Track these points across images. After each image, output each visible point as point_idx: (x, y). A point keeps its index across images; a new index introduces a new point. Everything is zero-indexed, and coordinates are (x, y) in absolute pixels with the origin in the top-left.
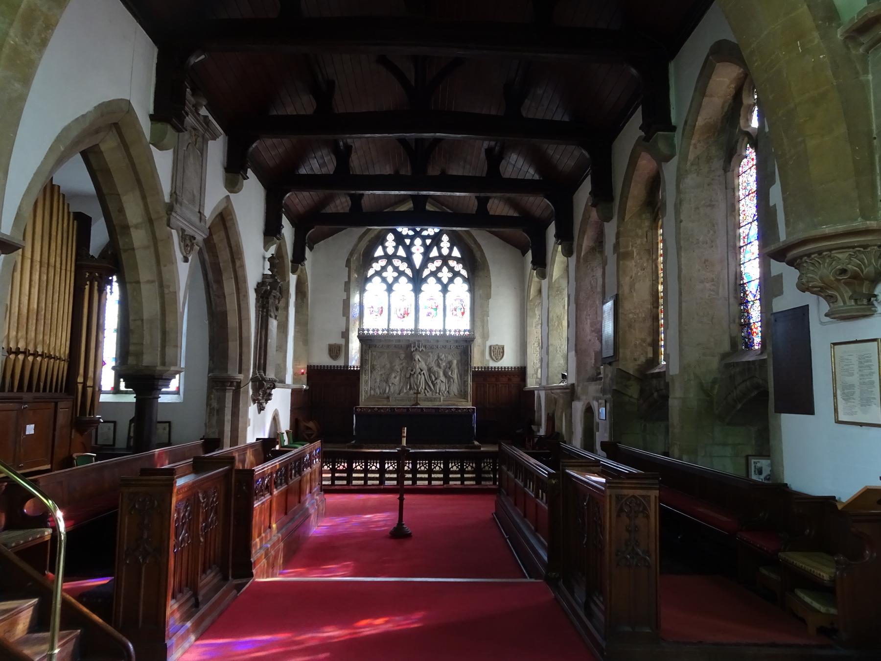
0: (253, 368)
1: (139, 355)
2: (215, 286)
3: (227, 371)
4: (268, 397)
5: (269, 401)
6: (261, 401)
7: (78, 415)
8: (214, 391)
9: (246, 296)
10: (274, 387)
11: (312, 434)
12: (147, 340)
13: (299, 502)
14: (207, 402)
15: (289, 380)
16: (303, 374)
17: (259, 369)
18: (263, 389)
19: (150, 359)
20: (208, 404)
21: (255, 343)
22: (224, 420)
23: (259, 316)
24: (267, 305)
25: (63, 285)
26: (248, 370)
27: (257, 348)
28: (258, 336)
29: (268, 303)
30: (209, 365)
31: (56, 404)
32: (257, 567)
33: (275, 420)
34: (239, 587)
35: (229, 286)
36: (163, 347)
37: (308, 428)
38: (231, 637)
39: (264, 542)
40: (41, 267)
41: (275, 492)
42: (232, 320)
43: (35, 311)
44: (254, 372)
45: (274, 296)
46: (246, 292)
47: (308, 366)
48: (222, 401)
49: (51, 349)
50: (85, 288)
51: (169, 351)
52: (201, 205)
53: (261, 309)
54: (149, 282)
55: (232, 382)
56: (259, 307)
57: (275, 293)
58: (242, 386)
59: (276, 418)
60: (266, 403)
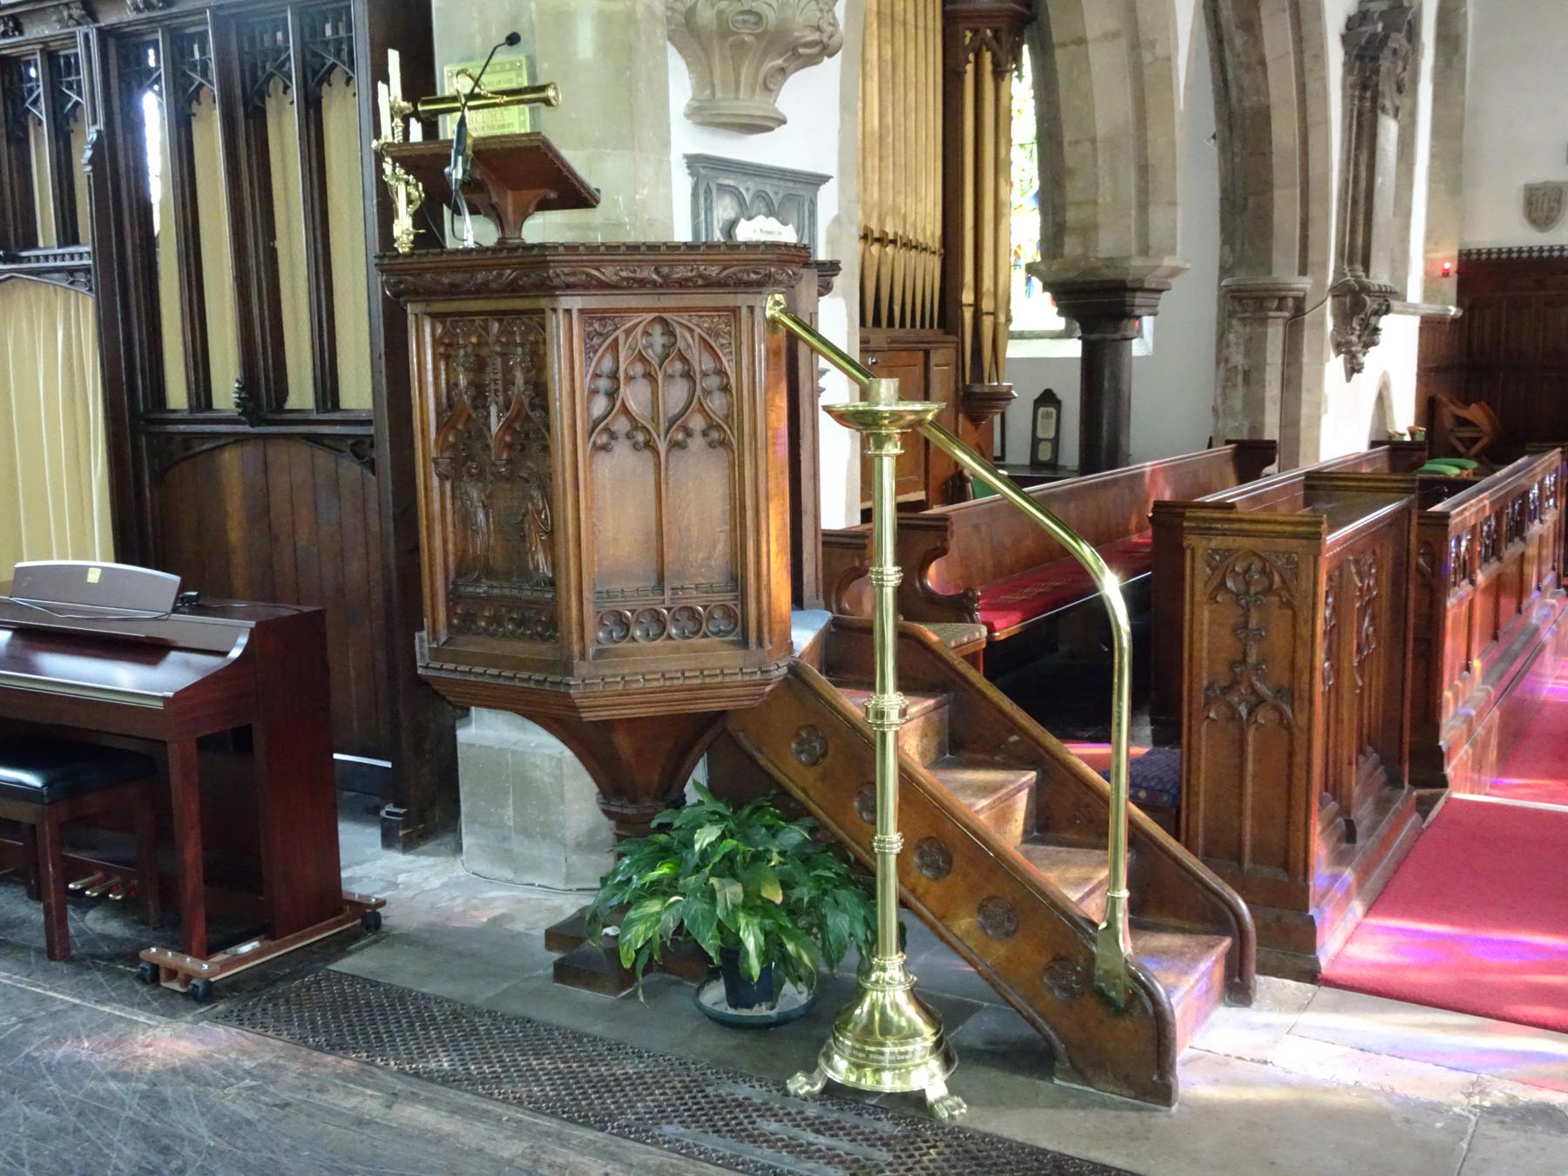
0: (1336, 261)
1: (1088, 230)
2: (1239, 39)
3: (1270, 272)
4: (1370, 336)
5: (1371, 349)
6: (1354, 349)
7: (968, 382)
8: (1234, 322)
9: (1320, 57)
10: (1388, 311)
11: (1475, 441)
12: (1104, 196)
13: (1519, 611)
14: (1219, 350)
15: (1414, 291)
16: (1446, 274)
17: (1351, 262)
18: (1362, 316)
20: (1221, 359)
21: (1340, 191)
22: (1263, 399)
23: (1352, 110)
24: (1374, 78)
25: (922, 66)
26: (1325, 266)
27: (1346, 205)
28: (1348, 169)
29: (1377, 72)
30: (1222, 259)
31: (927, 353)
32: (1454, 762)
34: (1424, 806)
35: (1276, 36)
36: (1143, 207)
37: (1462, 422)
38: (1452, 924)
39: (1460, 704)
40: (879, 26)
41: (1480, 578)
42: (1284, 132)
43: (877, 135)
44: (1339, 271)
45: (1395, 52)
47: (1461, 253)
48: (1255, 348)
49: (908, 227)
50: (965, 72)
51: (1157, 216)
53: (1357, 93)
55: (1282, 299)
56: (1353, 87)
57: (1398, 40)
58: (1308, 306)
59: (1385, 393)
60: (1364, 354)
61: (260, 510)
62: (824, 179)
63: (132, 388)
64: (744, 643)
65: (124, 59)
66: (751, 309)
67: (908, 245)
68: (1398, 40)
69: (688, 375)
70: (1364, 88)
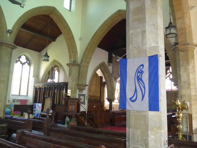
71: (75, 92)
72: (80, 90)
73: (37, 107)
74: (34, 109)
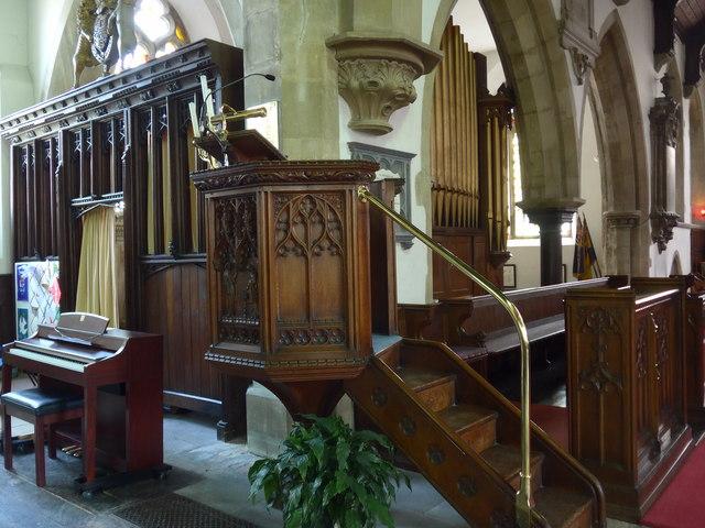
4: (669, 236)
9: (640, 124)
15: (688, 219)
17: (658, 205)
19: (551, 192)
31: (473, 238)
33: (676, 262)
36: (564, 177)
46: (640, 118)
52: (590, 21)
54: (545, 110)
61: (179, 295)
62: (414, 155)
63: (136, 245)
64: (348, 346)
65: (140, 121)
66: (351, 191)
67: (464, 194)
68: (672, 117)
69: (322, 222)
70: (659, 136)
71: (322, 125)
72: (369, 98)
73: (33, 286)
74: (20, 305)
